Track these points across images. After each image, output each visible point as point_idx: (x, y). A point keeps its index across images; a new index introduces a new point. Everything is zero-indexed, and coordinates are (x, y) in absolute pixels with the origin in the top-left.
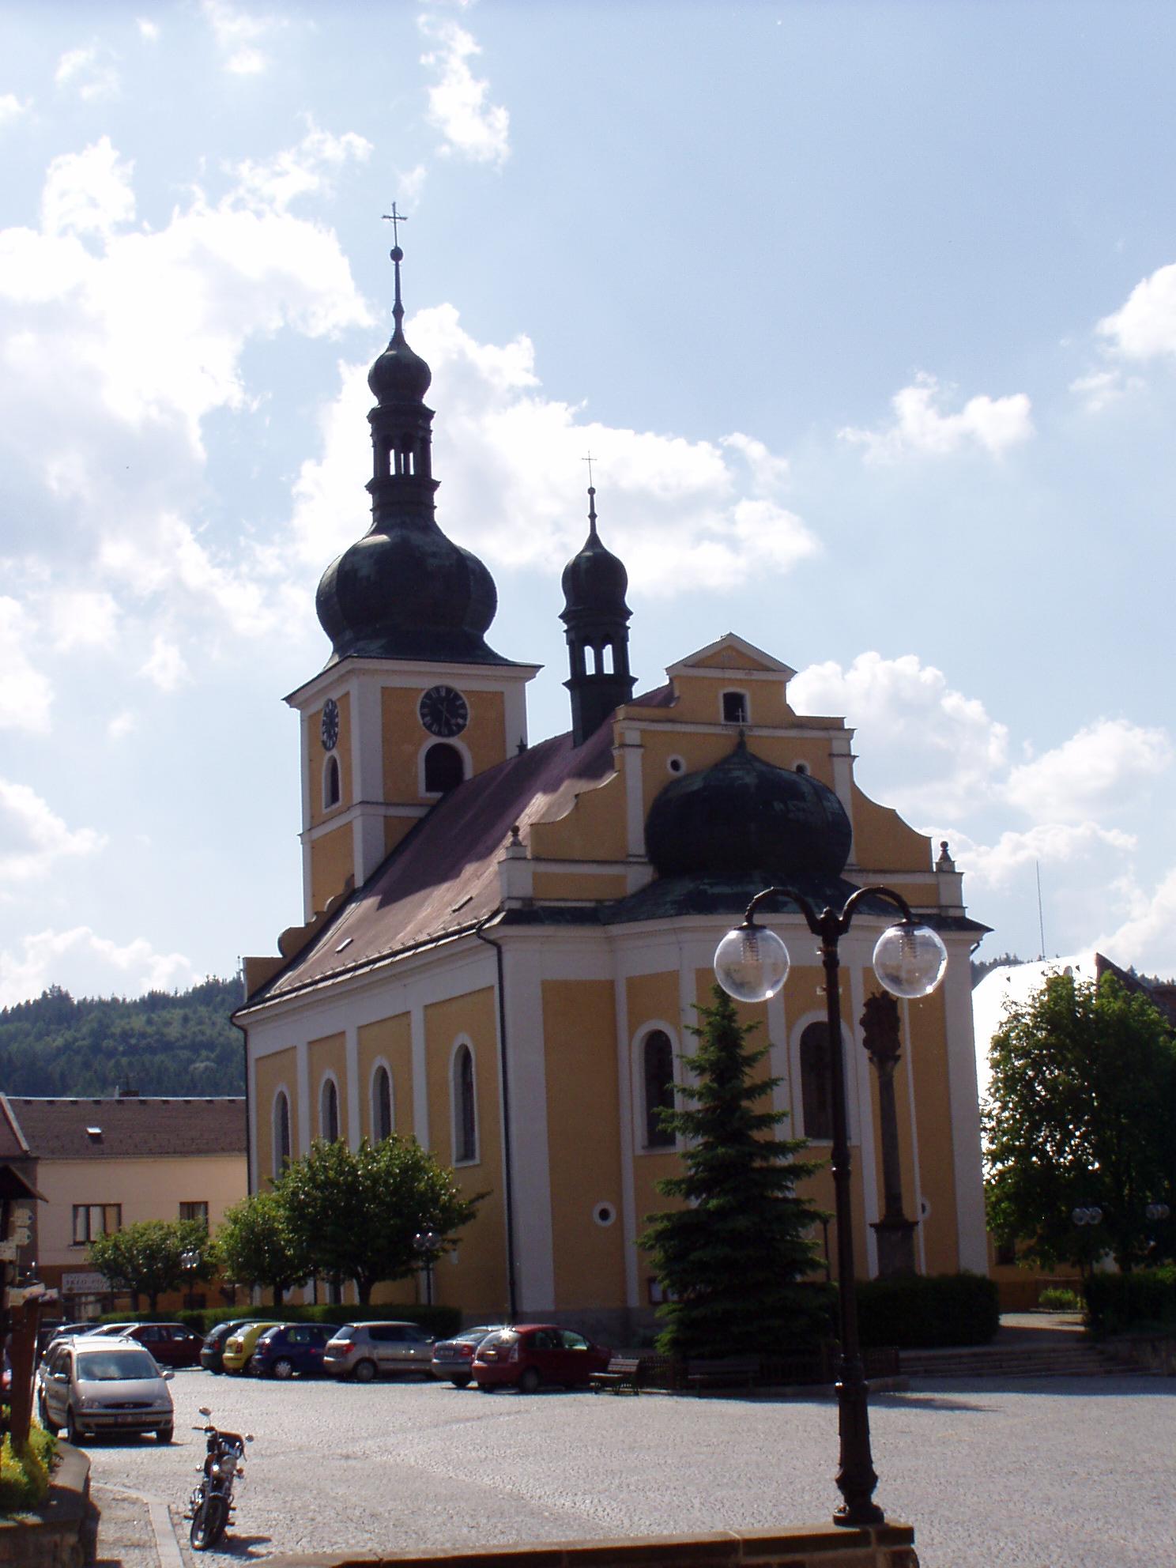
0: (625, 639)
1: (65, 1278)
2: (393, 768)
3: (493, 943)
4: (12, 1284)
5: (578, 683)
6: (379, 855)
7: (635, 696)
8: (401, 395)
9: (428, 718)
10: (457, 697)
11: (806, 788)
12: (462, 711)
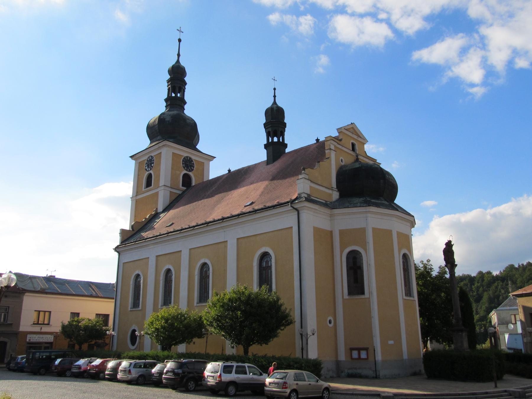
1: (29, 336)
2: (174, 177)
3: (296, 209)
4: (496, 345)
6: (168, 202)
7: (286, 152)
8: (177, 77)
10: (192, 161)
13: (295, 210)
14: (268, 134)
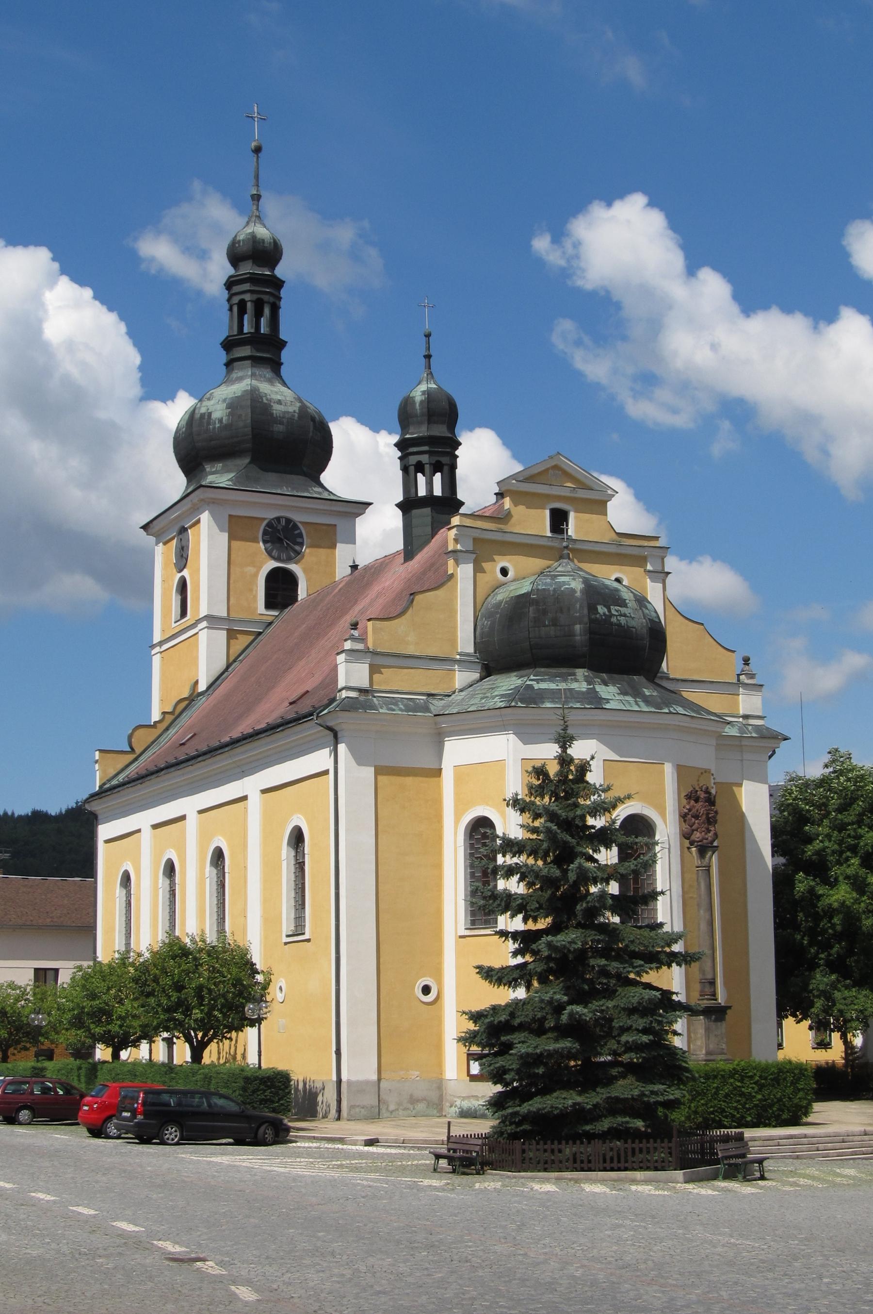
0: (453, 467)
5: (408, 505)
6: (222, 663)
10: (295, 527)
11: (626, 595)
13: (328, 732)
14: (409, 471)
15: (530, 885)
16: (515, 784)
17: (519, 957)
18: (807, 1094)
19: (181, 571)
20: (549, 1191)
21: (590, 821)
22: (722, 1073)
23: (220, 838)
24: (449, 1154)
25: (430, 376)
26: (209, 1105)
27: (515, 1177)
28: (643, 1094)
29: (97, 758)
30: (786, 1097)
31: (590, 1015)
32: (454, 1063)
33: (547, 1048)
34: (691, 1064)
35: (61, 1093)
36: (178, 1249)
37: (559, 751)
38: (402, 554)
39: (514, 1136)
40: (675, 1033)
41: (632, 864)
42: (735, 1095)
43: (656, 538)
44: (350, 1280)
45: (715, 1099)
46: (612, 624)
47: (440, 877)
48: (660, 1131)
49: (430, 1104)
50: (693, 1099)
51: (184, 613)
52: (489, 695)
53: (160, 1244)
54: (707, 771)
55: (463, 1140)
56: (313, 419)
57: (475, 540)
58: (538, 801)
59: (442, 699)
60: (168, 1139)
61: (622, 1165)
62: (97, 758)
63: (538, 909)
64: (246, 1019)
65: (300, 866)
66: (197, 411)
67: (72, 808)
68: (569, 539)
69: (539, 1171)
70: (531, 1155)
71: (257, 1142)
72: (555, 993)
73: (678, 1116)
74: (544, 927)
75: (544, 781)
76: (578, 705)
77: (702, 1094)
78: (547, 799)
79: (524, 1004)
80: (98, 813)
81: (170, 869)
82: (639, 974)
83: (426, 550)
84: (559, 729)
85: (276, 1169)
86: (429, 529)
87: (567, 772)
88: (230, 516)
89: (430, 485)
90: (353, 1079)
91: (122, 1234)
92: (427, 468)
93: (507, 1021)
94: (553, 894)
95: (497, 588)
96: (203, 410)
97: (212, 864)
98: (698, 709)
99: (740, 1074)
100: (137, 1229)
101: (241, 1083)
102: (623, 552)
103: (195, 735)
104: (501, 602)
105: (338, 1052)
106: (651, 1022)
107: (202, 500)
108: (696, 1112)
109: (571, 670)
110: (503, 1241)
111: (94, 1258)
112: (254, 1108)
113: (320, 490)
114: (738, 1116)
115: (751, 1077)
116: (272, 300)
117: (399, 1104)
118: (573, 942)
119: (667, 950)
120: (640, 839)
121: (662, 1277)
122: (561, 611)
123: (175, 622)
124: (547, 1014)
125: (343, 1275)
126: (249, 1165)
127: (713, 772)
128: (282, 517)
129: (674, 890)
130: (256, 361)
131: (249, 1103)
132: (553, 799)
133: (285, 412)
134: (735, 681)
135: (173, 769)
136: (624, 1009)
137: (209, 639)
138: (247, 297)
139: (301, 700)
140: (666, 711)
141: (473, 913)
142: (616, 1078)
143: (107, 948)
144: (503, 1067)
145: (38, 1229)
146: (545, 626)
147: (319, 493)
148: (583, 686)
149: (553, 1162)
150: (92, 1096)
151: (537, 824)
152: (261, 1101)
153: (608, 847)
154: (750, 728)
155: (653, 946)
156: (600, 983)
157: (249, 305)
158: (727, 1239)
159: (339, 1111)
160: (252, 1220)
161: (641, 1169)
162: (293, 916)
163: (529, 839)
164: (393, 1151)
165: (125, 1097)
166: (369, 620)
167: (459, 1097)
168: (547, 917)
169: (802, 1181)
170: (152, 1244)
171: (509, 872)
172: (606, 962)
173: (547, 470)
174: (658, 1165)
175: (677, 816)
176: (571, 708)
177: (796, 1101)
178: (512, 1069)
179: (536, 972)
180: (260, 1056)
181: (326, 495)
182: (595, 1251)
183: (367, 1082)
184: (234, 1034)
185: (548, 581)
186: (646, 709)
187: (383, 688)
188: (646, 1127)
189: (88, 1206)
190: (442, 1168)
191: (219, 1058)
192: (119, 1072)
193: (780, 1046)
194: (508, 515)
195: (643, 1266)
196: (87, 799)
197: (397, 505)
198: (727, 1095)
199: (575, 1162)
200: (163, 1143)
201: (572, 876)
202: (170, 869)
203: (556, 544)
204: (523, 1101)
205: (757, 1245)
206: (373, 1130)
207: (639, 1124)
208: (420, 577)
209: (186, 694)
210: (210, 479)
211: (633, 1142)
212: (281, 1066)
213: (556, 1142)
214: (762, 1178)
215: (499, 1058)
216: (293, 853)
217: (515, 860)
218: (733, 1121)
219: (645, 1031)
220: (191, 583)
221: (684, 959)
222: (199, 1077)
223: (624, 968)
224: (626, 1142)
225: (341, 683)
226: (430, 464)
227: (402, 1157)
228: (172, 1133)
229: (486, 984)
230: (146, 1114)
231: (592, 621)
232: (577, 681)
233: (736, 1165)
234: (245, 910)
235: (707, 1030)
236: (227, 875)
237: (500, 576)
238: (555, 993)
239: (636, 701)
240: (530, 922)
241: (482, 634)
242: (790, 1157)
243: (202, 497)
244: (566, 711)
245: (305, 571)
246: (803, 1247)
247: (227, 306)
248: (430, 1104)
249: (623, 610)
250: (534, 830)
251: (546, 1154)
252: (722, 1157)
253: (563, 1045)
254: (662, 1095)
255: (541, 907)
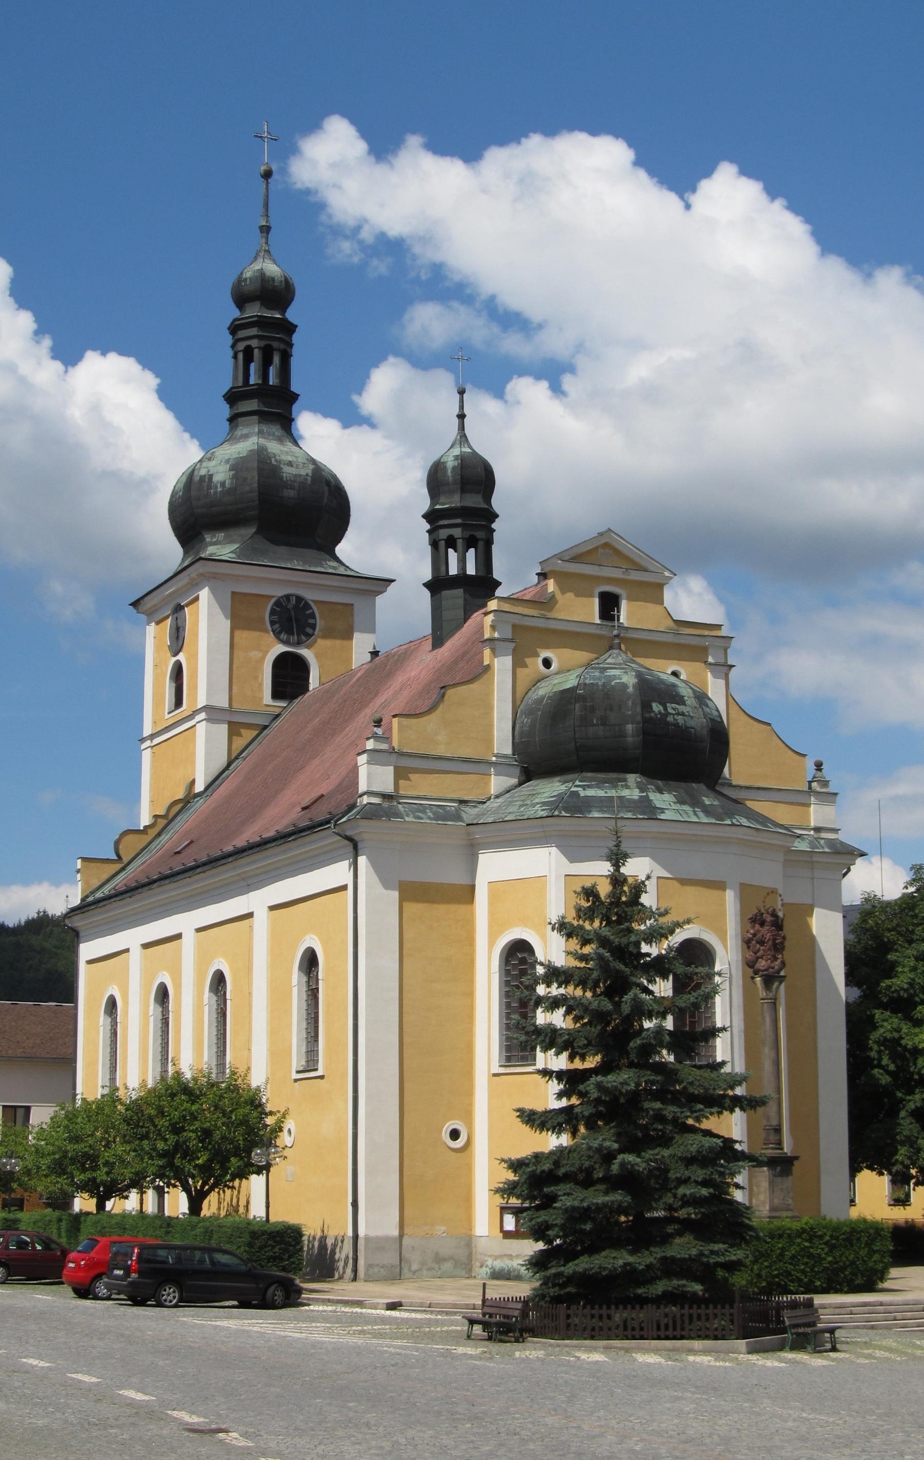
0: (489, 542)
5: (438, 585)
6: (222, 760)
9: (277, 626)
10: (307, 606)
11: (685, 691)
12: (311, 621)
13: (346, 842)
14: (439, 546)
15: (576, 1019)
16: (558, 904)
17: (564, 1099)
18: (883, 1256)
19: (175, 655)
20: (597, 1361)
21: (645, 948)
22: (789, 1232)
23: (221, 960)
24: (484, 1319)
25: (463, 439)
26: (213, 1262)
27: (558, 1346)
28: (701, 1254)
29: (79, 866)
30: (864, 1257)
31: (644, 1165)
32: (485, 1216)
33: (595, 1201)
34: (755, 1222)
35: (39, 1248)
36: (195, 1419)
37: (612, 869)
38: (430, 640)
39: (557, 1300)
40: (737, 1186)
41: (692, 998)
42: (803, 1257)
43: (719, 627)
44: (390, 1452)
45: (780, 1261)
46: (668, 724)
47: (471, 1008)
48: (720, 1295)
49: (457, 1263)
50: (755, 1261)
51: (178, 702)
52: (528, 802)
53: (175, 1414)
54: (773, 892)
55: (500, 1304)
56: (328, 483)
57: (515, 627)
58: (587, 926)
59: (475, 807)
60: (165, 1300)
61: (670, 1333)
62: (79, 866)
63: (586, 1046)
64: (252, 1165)
65: (313, 994)
66: (196, 473)
67: (33, 919)
68: (621, 627)
69: (585, 1339)
70: (577, 1321)
71: (265, 1304)
72: (604, 1140)
73: (739, 1280)
74: (593, 1066)
75: (594, 903)
76: (629, 815)
77: (765, 1255)
78: (597, 923)
79: (570, 1151)
80: (78, 929)
81: (163, 995)
82: (698, 1120)
83: (457, 636)
84: (611, 844)
85: (290, 1334)
86: (461, 613)
87: (621, 893)
88: (233, 593)
89: (462, 561)
90: (372, 1234)
91: (132, 1403)
92: (460, 543)
93: (551, 1171)
94: (604, 1030)
95: (539, 681)
96: (203, 472)
97: (211, 990)
98: (764, 820)
99: (810, 1234)
100: (146, 1398)
101: (247, 1238)
102: (682, 641)
103: (192, 842)
104: (542, 698)
105: (355, 1204)
106: (712, 1173)
107: (201, 575)
108: (759, 1276)
109: (621, 776)
110: (553, 1413)
111: (105, 1429)
112: (262, 1266)
113: (335, 564)
114: (806, 1280)
115: (821, 1237)
116: (282, 346)
117: (423, 1263)
118: (625, 1083)
119: (730, 1093)
120: (700, 969)
121: (730, 1452)
122: (611, 710)
123: (169, 713)
124: (595, 1163)
125: (382, 1448)
126: (259, 1329)
127: (780, 892)
128: (292, 595)
129: (735, 1024)
130: (264, 417)
131: (256, 1261)
132: (604, 923)
133: (296, 476)
134: (806, 788)
135: (167, 881)
136: (681, 1159)
137: (208, 732)
138: (254, 343)
139: (316, 805)
140: (729, 822)
141: (508, 1048)
142: (672, 1236)
143: (89, 1084)
144: (546, 1222)
145: (38, 1397)
146: (593, 725)
147: (334, 568)
148: (635, 794)
149: (601, 1329)
150: (79, 1252)
151: (587, 950)
152: (269, 1259)
153: (665, 977)
154: (822, 842)
155: (714, 1089)
156: (655, 1130)
157: (257, 353)
158: (797, 1414)
159: (355, 1270)
160: (273, 1389)
161: (699, 1337)
162: (304, 1049)
163: (576, 967)
164: (419, 1316)
165: (116, 1254)
166: (394, 716)
167: (490, 1256)
168: (597, 1054)
169: (878, 1353)
170: (167, 1414)
171: (554, 1004)
172: (661, 1106)
173: (597, 548)
174: (719, 1333)
175: (740, 942)
176: (622, 818)
177: (871, 1264)
178: (556, 1225)
179: (583, 1116)
180: (268, 1207)
181: (342, 570)
182: (655, 1424)
183: (387, 1239)
184: (237, 1183)
185: (597, 674)
186: (705, 820)
187: (409, 793)
188: (705, 1291)
189: (88, 1373)
190: (478, 1335)
191: (219, 1209)
192: (105, 1224)
193: (852, 1202)
194: (552, 598)
195: (708, 1441)
196: (68, 913)
197: (425, 585)
198: (793, 1257)
199: (625, 1329)
200: (160, 1305)
201: (626, 1009)
202: (163, 995)
203: (604, 632)
204: (567, 1261)
205: (831, 1420)
206: (395, 1292)
207: (697, 1288)
208: (452, 666)
209: (180, 795)
210: (210, 550)
211: (691, 1308)
212: (292, 1219)
213: (605, 1307)
214: (834, 1349)
215: (542, 1212)
216: (305, 979)
217: (562, 991)
218: (800, 1286)
219: (705, 1183)
220: (188, 668)
221: (749, 1104)
222: (198, 1231)
223: (682, 1112)
224: (682, 1308)
225: (363, 787)
226: (463, 539)
227: (429, 1322)
228: (170, 1294)
229: (526, 1129)
230: (141, 1273)
231: (645, 721)
232: (627, 787)
233: (805, 1335)
234: (249, 1041)
235: (772, 1183)
236: (228, 1002)
237: (542, 667)
238: (604, 1140)
239: (694, 812)
240: (577, 1060)
241: (522, 734)
242: (864, 1327)
243: (201, 571)
244: (620, 823)
245: (318, 657)
246: (882, 1423)
247: (231, 353)
248: (457, 1263)
249: (681, 708)
250: (583, 958)
251: (594, 1320)
252: (790, 1325)
253: (614, 1198)
254: (723, 1255)
255: (589, 1044)
